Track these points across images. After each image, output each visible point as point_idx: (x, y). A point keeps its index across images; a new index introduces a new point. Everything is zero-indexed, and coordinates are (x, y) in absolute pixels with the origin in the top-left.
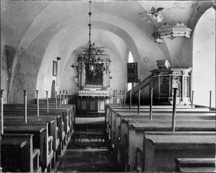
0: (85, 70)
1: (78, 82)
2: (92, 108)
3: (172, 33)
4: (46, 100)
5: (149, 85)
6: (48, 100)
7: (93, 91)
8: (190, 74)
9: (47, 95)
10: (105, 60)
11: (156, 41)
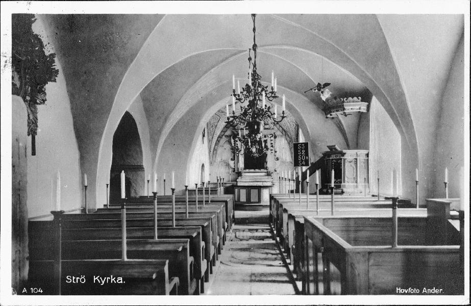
1: (235, 166)
3: (344, 109)
7: (249, 178)
8: (367, 155)
10: (270, 136)
11: (327, 118)
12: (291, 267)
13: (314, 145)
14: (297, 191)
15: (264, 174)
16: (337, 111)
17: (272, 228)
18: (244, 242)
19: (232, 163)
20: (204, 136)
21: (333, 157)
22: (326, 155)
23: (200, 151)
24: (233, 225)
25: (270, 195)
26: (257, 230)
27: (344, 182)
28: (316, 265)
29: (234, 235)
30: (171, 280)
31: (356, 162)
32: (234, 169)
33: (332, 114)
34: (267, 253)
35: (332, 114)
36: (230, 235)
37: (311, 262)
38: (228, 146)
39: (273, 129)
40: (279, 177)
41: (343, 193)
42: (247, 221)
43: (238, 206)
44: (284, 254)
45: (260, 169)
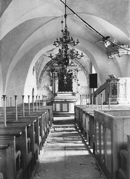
0: (23, 46)
1: (52, 90)
3: (118, 53)
4: (33, 104)
5: (105, 90)
6: (6, 116)
10: (74, 70)
11: (109, 58)
12: (88, 143)
13: (101, 75)
14: (91, 104)
15: (71, 94)
16: (115, 54)
17: (76, 126)
18: (60, 133)
19: (51, 88)
20: (34, 70)
21: (112, 82)
22: (108, 81)
23: (31, 80)
24: (53, 124)
25: (75, 106)
26: (67, 127)
27: (119, 97)
28: (100, 142)
29: (54, 130)
30: (16, 152)
32: (52, 91)
33: (112, 55)
34: (73, 138)
35: (112, 55)
36: (52, 130)
37: (98, 141)
38: (48, 77)
39: (76, 66)
40: (79, 95)
41: (118, 103)
42: (61, 122)
43: (56, 114)
44: (83, 138)
45: (68, 91)
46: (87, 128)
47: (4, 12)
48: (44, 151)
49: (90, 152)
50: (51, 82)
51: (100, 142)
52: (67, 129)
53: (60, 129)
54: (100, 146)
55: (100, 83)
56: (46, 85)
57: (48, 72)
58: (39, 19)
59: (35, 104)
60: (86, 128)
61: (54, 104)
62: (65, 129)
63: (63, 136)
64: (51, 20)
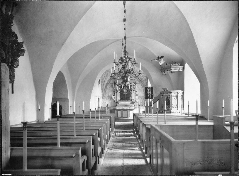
1: (115, 99)
2: (125, 116)
3: (171, 70)
8: (183, 93)
9: (231, 158)
11: (162, 74)
12: (144, 151)
14: (147, 112)
16: (168, 70)
19: (113, 97)
20: (99, 83)
22: (162, 93)
23: (97, 91)
24: (114, 129)
25: (133, 114)
26: (126, 132)
28: (157, 149)
29: (114, 134)
31: (177, 97)
38: (111, 89)
41: (170, 112)
43: (117, 119)
44: (140, 144)
46: (144, 137)
47: (70, 34)
48: (104, 159)
49: (146, 161)
50: (114, 93)
51: (157, 149)
52: (126, 134)
53: (120, 134)
54: (157, 153)
55: (155, 95)
56: (109, 95)
57: (111, 85)
58: (103, 41)
59: (101, 111)
60: (142, 136)
61: (116, 111)
62: (124, 134)
63: (122, 141)
64: (113, 42)
